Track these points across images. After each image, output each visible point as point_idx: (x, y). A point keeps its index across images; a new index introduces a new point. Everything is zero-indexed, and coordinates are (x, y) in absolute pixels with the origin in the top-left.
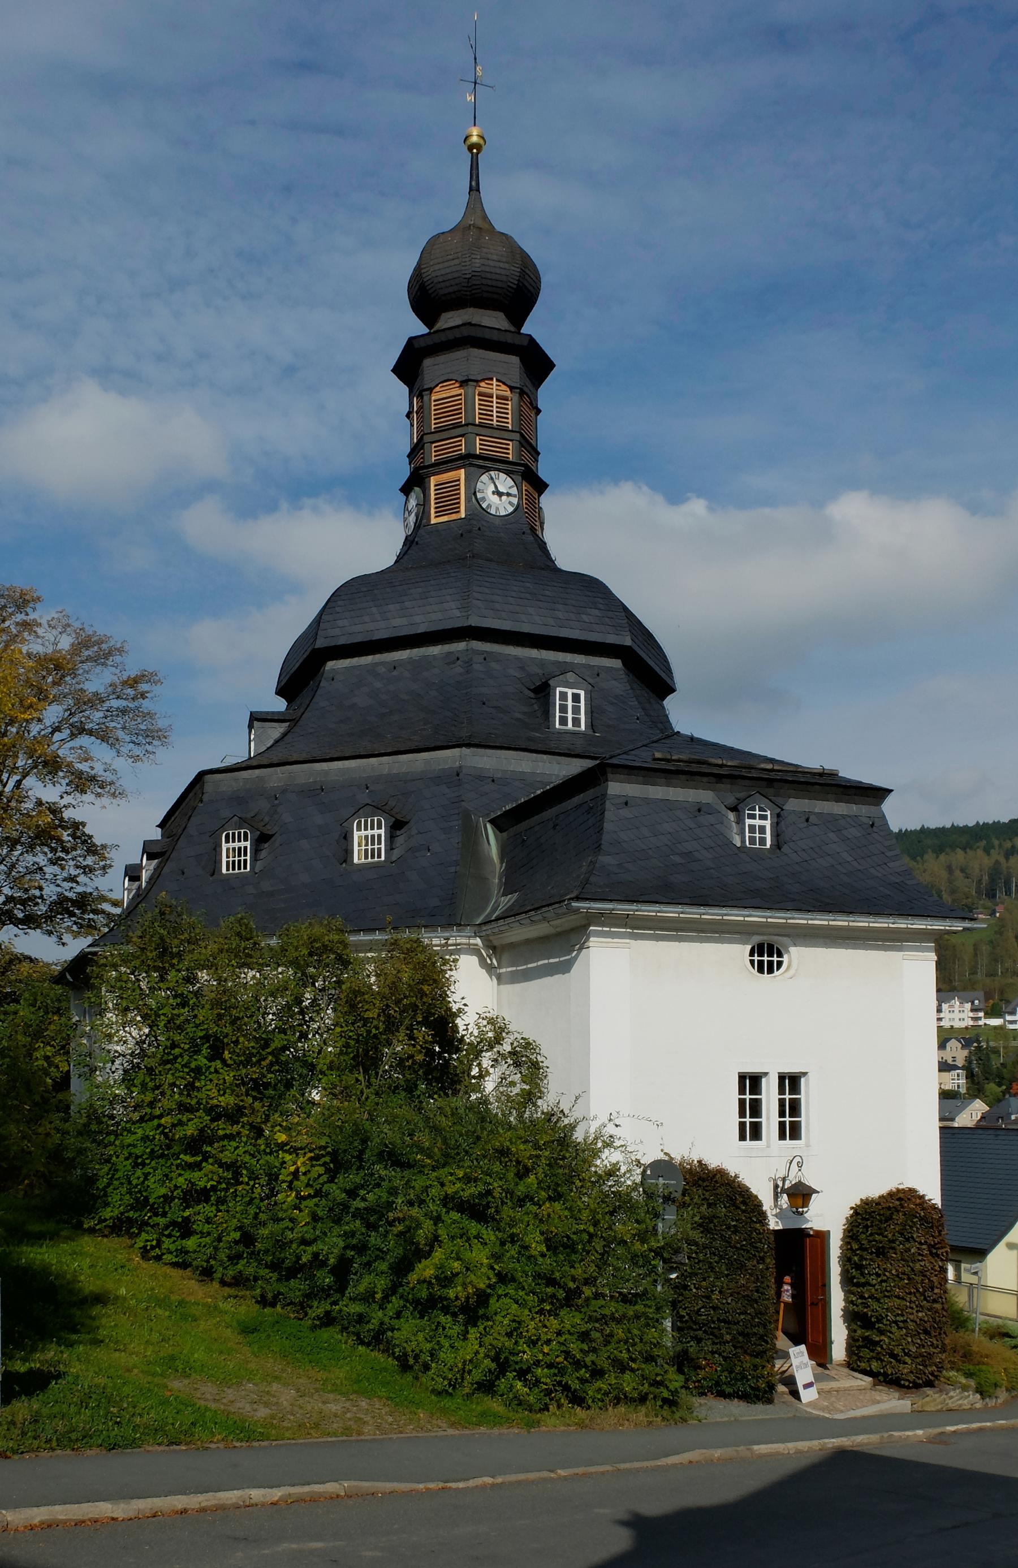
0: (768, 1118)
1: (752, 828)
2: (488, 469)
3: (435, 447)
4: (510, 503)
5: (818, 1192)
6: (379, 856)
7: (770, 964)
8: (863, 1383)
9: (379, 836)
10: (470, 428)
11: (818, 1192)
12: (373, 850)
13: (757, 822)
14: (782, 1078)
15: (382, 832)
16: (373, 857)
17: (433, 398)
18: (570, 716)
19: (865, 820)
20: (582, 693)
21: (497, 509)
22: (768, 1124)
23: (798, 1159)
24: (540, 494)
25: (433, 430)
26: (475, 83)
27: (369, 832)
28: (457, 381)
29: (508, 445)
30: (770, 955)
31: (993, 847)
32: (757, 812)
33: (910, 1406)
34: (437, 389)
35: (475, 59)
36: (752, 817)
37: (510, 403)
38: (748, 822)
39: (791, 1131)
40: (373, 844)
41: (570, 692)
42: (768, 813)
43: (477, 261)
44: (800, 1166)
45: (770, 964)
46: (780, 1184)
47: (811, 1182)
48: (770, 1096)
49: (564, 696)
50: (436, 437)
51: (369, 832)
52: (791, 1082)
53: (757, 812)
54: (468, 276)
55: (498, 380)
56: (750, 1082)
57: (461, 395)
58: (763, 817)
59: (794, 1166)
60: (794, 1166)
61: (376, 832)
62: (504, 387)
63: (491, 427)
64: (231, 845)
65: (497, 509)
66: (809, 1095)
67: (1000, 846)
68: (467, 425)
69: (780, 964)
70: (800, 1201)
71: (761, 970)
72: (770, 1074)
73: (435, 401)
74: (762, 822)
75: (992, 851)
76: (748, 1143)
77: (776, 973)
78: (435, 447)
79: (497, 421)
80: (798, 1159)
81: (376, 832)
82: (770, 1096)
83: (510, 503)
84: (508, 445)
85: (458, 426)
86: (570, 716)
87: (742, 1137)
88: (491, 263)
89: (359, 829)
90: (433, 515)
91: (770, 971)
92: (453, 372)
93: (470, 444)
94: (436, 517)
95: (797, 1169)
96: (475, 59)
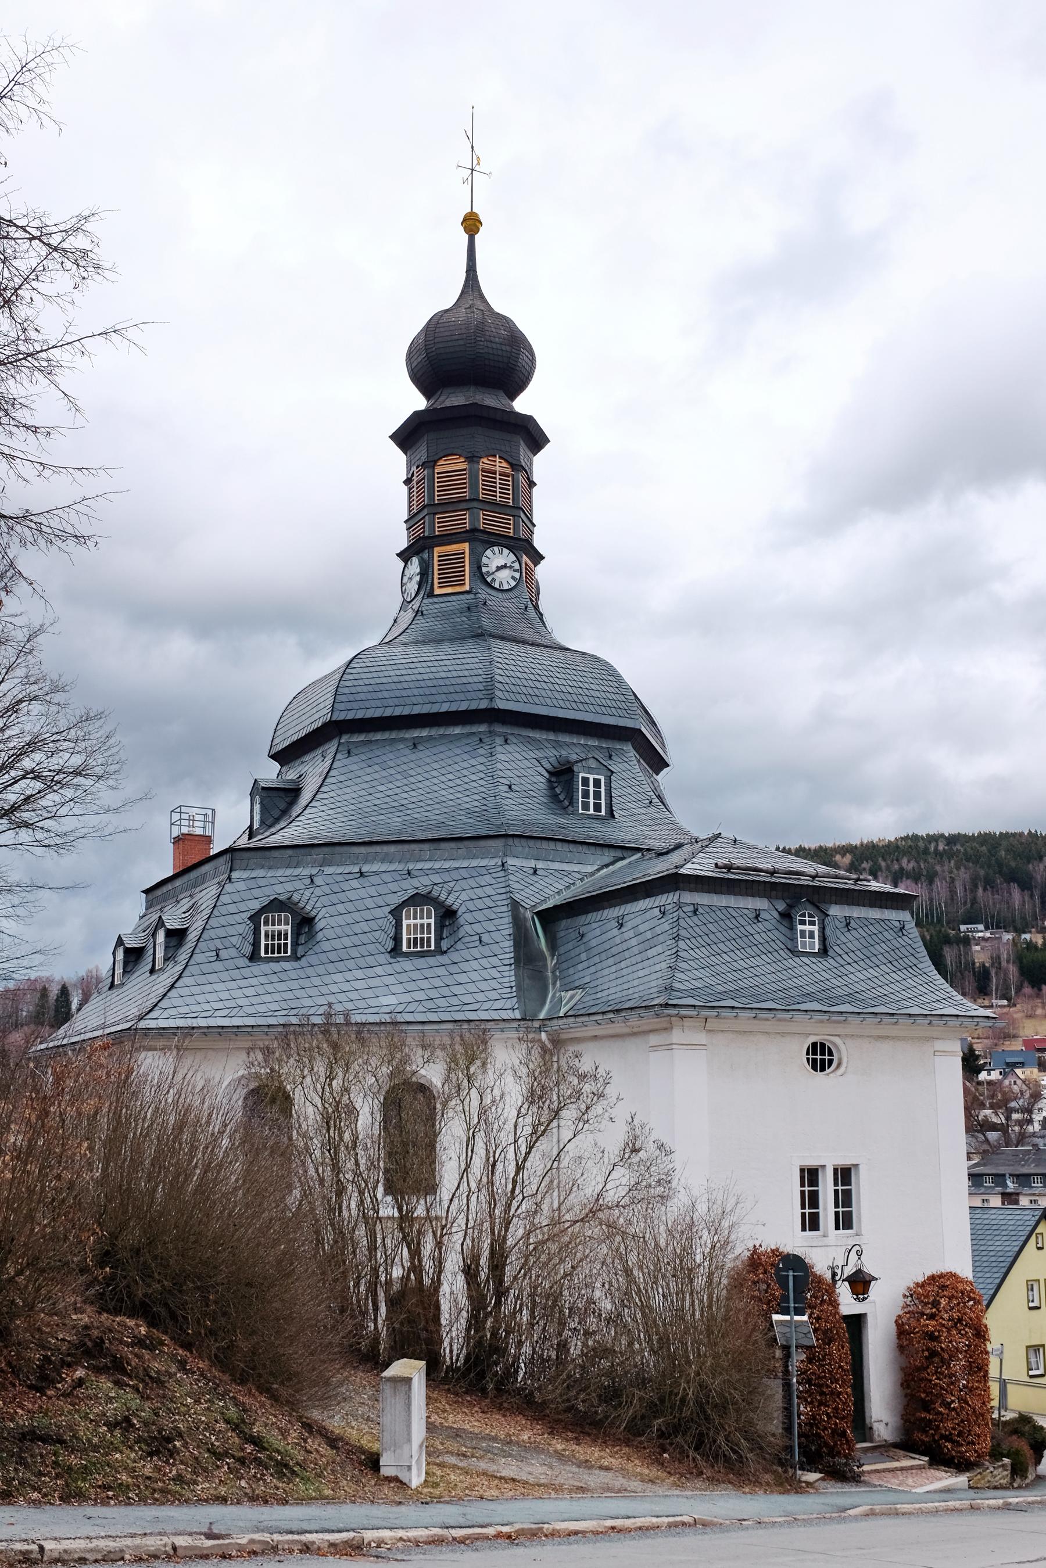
0: (825, 1209)
1: (803, 932)
2: (493, 544)
3: (438, 518)
4: (513, 578)
5: (877, 1279)
6: (429, 946)
7: (823, 1061)
8: (922, 1463)
9: (429, 925)
10: (475, 504)
11: (877, 1279)
12: (422, 939)
13: (807, 928)
14: (836, 1170)
15: (432, 921)
16: (422, 946)
17: (436, 471)
18: (591, 800)
19: (897, 924)
20: (602, 778)
21: (501, 583)
22: (826, 1216)
23: (857, 1248)
24: (536, 564)
25: (436, 502)
26: (472, 170)
27: (419, 921)
28: (460, 456)
29: (510, 520)
30: (823, 1053)
31: (880, 869)
32: (807, 919)
33: (967, 1483)
34: (441, 462)
35: (472, 147)
36: (803, 923)
37: (510, 479)
38: (800, 927)
39: (844, 1221)
40: (422, 933)
41: (591, 777)
42: (816, 919)
43: (482, 343)
44: (859, 1254)
45: (823, 1061)
46: (839, 1272)
47: (870, 1269)
48: (827, 1189)
49: (585, 782)
50: (440, 509)
51: (419, 921)
52: (844, 1175)
53: (807, 919)
54: (473, 357)
55: (500, 457)
56: (810, 1175)
57: (465, 470)
58: (812, 923)
59: (853, 1256)
60: (853, 1256)
61: (425, 921)
62: (504, 464)
63: (494, 504)
64: (270, 928)
65: (501, 583)
66: (863, 1188)
67: (888, 868)
68: (470, 500)
69: (831, 1062)
70: (860, 1289)
71: (814, 1068)
72: (827, 1167)
73: (438, 473)
74: (812, 928)
75: (879, 873)
76: (808, 1233)
77: (828, 1071)
78: (438, 518)
79: (500, 497)
80: (857, 1248)
81: (425, 921)
82: (827, 1189)
83: (513, 578)
84: (510, 520)
85: (462, 501)
86: (591, 800)
87: (804, 1229)
88: (494, 346)
89: (408, 918)
90: (436, 585)
91: (823, 1069)
92: (458, 448)
93: (474, 518)
94: (440, 587)
95: (857, 1257)
96: (472, 147)
